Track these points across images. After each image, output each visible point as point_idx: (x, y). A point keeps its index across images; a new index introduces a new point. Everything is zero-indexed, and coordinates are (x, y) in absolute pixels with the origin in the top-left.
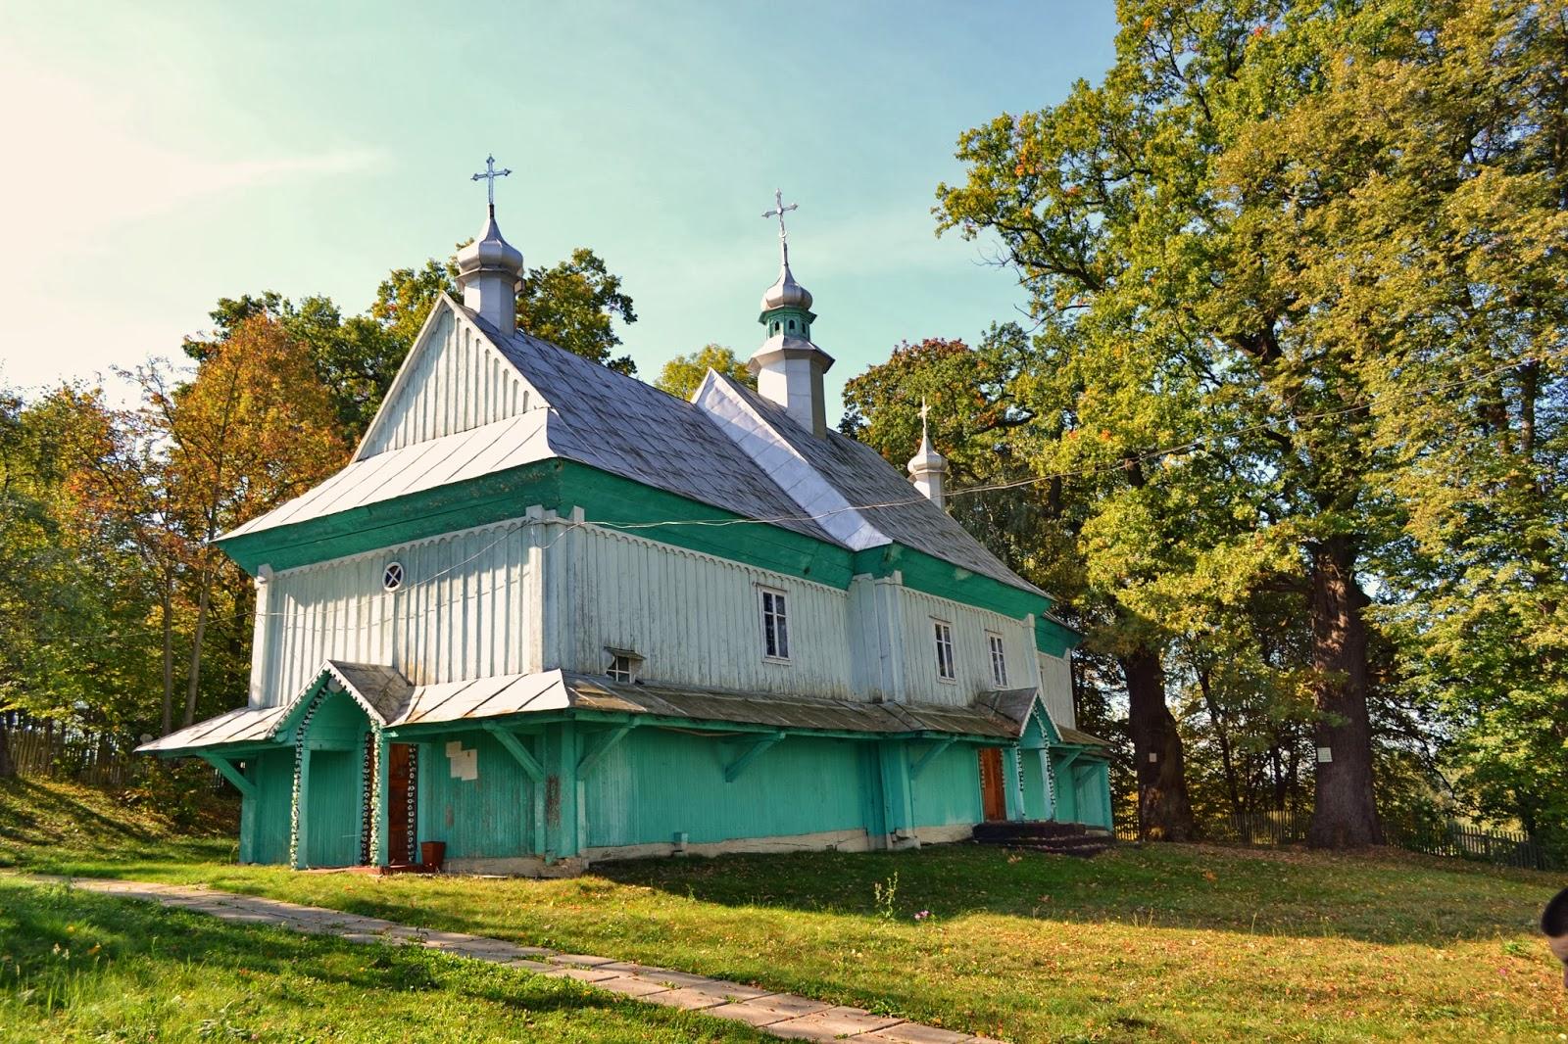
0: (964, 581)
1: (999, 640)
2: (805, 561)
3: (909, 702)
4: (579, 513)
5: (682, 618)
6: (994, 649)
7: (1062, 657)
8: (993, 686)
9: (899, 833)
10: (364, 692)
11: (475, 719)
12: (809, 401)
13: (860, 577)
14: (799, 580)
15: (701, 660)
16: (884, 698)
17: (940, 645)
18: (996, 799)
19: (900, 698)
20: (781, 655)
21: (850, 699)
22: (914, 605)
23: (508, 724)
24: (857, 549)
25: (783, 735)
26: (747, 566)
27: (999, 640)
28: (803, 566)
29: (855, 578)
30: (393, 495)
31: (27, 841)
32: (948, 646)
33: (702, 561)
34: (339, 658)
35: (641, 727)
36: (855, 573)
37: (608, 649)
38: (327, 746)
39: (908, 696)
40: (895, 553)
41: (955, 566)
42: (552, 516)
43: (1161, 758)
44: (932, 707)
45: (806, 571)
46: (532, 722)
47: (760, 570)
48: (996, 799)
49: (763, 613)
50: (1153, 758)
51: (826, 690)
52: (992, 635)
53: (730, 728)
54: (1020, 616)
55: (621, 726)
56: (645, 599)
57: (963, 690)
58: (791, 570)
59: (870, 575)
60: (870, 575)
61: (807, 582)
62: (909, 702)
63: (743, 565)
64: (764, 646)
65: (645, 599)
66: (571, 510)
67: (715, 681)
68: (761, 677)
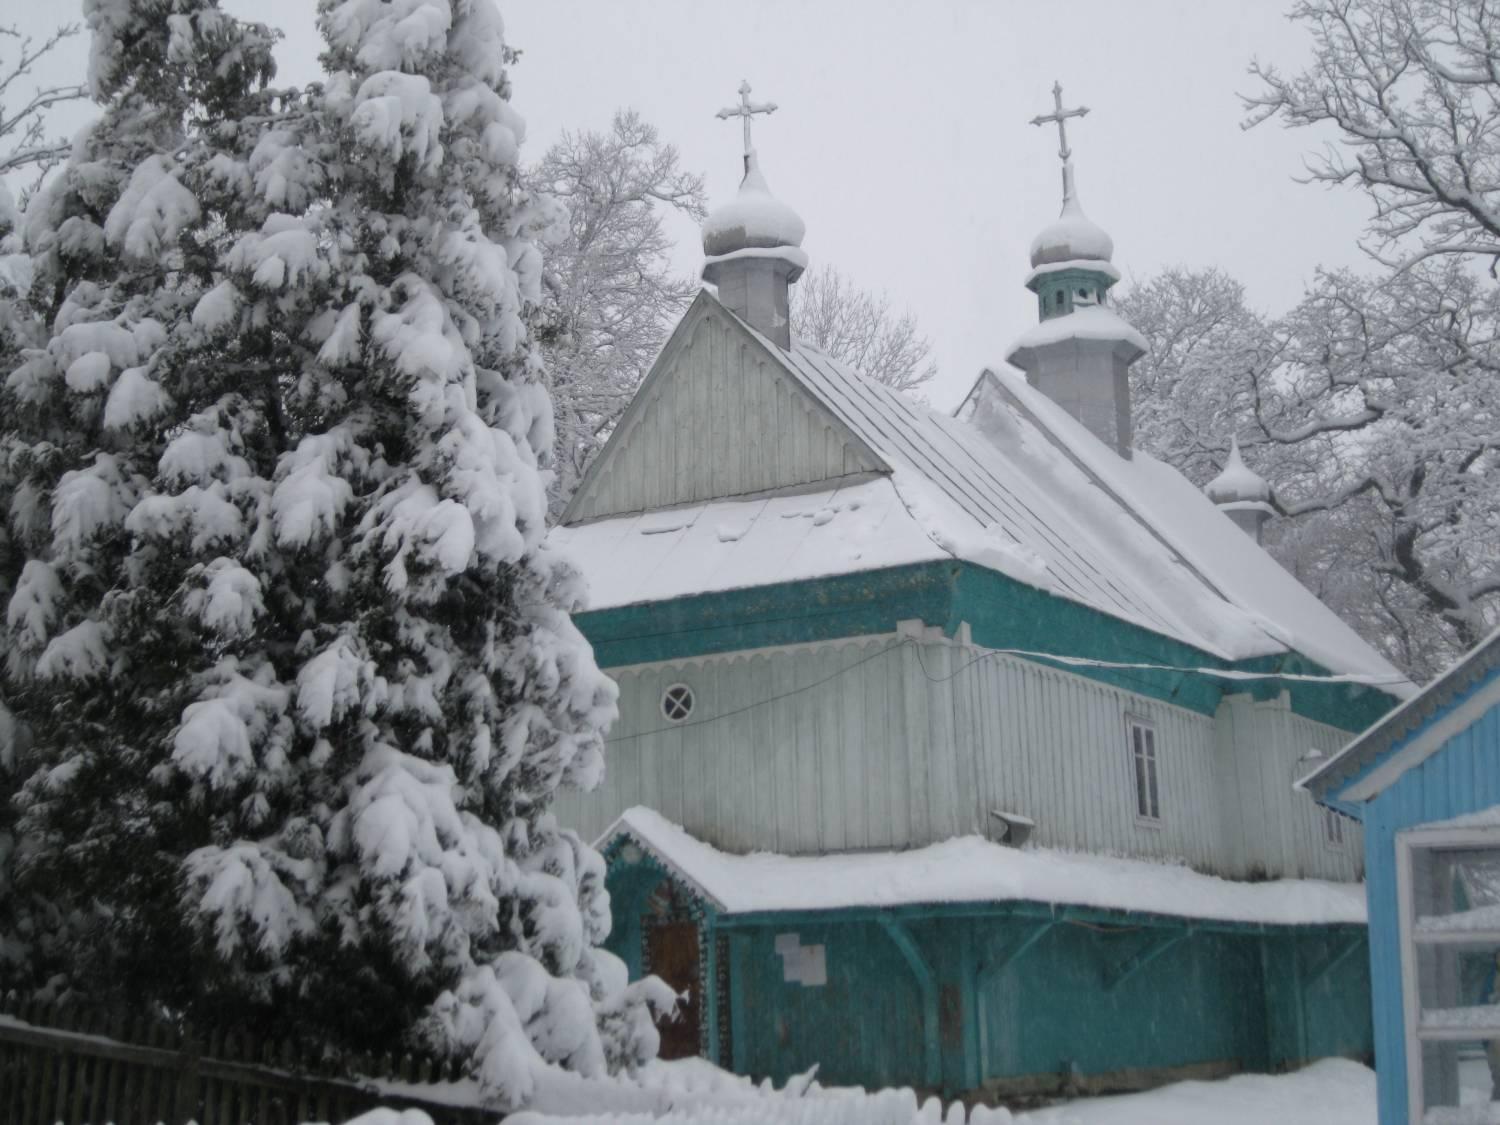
14: (1166, 705)
17: (1139, 762)
29: (1225, 698)
45: (1175, 693)
49: (1133, 756)
61: (1175, 707)
63: (1113, 689)
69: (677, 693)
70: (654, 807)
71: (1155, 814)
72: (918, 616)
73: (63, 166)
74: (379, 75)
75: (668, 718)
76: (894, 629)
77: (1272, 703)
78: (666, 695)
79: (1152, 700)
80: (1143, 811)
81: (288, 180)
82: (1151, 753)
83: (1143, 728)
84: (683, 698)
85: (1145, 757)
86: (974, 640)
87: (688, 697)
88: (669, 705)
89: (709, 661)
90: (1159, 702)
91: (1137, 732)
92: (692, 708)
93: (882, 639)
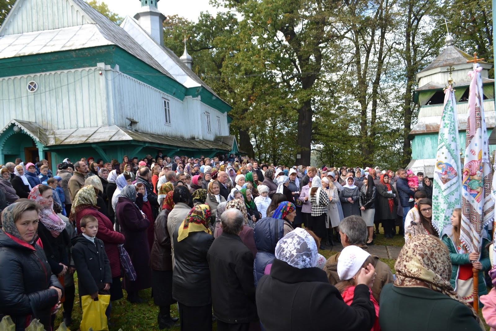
0: (214, 100)
1: (168, 103)
2: (174, 90)
4: (117, 67)
5: (145, 107)
8: (218, 135)
10: (33, 132)
13: (187, 97)
14: (172, 97)
15: (150, 123)
16: (196, 137)
17: (166, 109)
19: (201, 138)
22: (123, 79)
23: (100, 145)
25: (179, 150)
27: (168, 103)
28: (174, 92)
29: (185, 97)
30: (50, 51)
31: (321, 135)
33: (129, 79)
34: (20, 119)
35: (147, 147)
36: (186, 95)
37: (127, 118)
38: (10, 153)
39: (203, 137)
40: (200, 90)
42: (109, 67)
45: (174, 94)
46: (77, 147)
49: (164, 108)
52: (165, 100)
55: (140, 146)
56: (135, 101)
59: (191, 96)
60: (191, 96)
61: (174, 97)
63: (159, 90)
64: (165, 121)
65: (135, 101)
66: (115, 65)
67: (154, 131)
69: (32, 83)
70: (348, 245)
71: (170, 122)
72: (103, 62)
73: (463, 216)
74: (431, 147)
75: (29, 91)
76: (96, 66)
77: (196, 98)
78: (28, 84)
79: (169, 95)
80: (167, 121)
81: (156, 5)
82: (168, 108)
83: (167, 101)
84: (34, 85)
85: (167, 109)
86: (120, 70)
87: (35, 84)
88: (29, 87)
89: (41, 75)
90: (171, 96)
91: (165, 102)
92: (28, 85)
93: (93, 68)
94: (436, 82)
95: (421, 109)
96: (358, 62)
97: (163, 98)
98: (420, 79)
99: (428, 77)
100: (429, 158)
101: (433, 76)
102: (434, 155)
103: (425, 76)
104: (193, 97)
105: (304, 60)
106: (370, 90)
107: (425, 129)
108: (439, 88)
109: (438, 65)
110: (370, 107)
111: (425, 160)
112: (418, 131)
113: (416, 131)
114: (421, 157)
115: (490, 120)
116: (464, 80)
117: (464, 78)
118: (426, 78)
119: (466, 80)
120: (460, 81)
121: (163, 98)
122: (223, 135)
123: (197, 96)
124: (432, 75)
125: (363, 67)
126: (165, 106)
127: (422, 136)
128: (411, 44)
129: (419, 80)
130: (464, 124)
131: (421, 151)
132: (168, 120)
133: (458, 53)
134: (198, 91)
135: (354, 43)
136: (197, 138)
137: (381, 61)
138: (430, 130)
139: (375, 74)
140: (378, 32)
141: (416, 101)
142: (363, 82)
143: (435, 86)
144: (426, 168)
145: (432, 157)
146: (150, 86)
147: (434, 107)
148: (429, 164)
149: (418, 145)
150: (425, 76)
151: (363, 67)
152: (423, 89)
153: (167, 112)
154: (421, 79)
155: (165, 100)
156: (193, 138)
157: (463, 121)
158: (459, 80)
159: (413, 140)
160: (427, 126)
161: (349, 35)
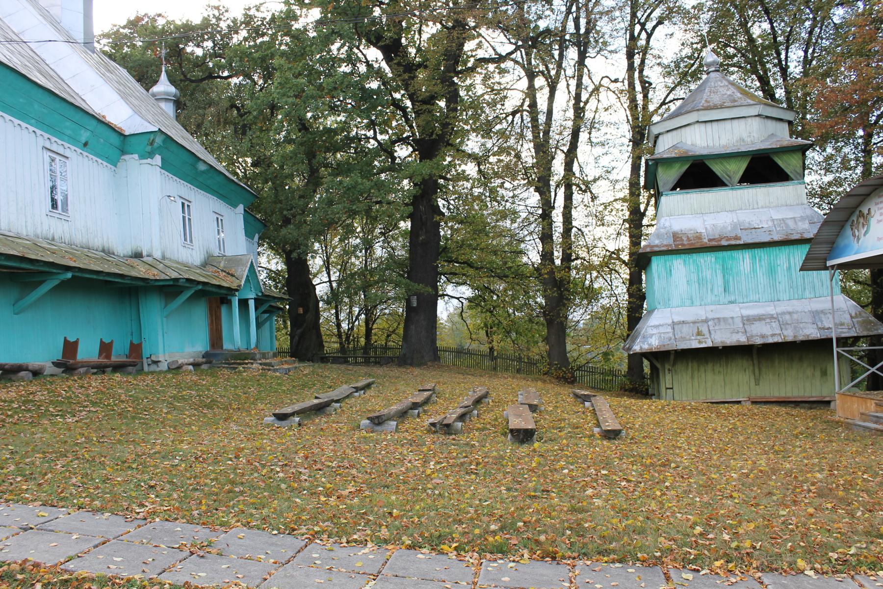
0: (203, 172)
1: (188, 206)
2: (84, 136)
3: (164, 258)
6: (218, 226)
7: (253, 239)
8: (216, 252)
9: (154, 358)
11: (573, 163)
12: (81, 17)
13: (126, 157)
14: (79, 151)
16: (144, 254)
17: (184, 218)
18: (216, 338)
19: (157, 254)
20: (63, 211)
21: (116, 254)
24: (127, 133)
26: (35, 130)
28: (83, 140)
29: (123, 157)
32: (189, 219)
41: (200, 159)
43: (306, 311)
44: (178, 263)
45: (86, 144)
47: (46, 135)
48: (216, 338)
49: (181, 215)
50: (301, 311)
51: (97, 242)
52: (218, 216)
53: (24, 266)
54: (235, 206)
57: (198, 253)
58: (73, 140)
59: (136, 156)
60: (136, 156)
61: (85, 154)
62: (164, 258)
63: (31, 128)
68: (46, 227)
71: (191, 241)
77: (149, 161)
80: (186, 240)
94: (689, 143)
95: (663, 199)
96: (533, 105)
97: (44, 148)
98: (657, 137)
99: (674, 133)
100: (682, 305)
101: (683, 130)
102: (691, 299)
103: (668, 131)
104: (142, 157)
105: (425, 103)
106: (558, 166)
107: (671, 241)
108: (697, 153)
109: (693, 108)
110: (560, 202)
111: (673, 310)
112: (657, 246)
113: (653, 246)
114: (667, 304)
115: (800, 224)
116: (746, 139)
117: (744, 135)
118: (670, 134)
119: (749, 140)
120: (737, 141)
121: (44, 148)
122: (229, 252)
123: (151, 155)
124: (681, 127)
125: (542, 118)
126: (183, 212)
127: (666, 257)
128: (636, 75)
129: (655, 142)
130: (750, 231)
131: (664, 289)
132: (187, 235)
133: (730, 86)
134: (152, 144)
135: (523, 67)
136: (148, 256)
137: (579, 111)
138: (683, 245)
139: (567, 133)
140: (572, 54)
141: (652, 183)
142: (543, 149)
143: (688, 151)
144: (676, 327)
145: (688, 302)
146: (177, 179)
147: (688, 195)
148: (682, 319)
149: (659, 277)
150: (668, 131)
151: (542, 118)
152: (665, 156)
153: (186, 223)
154: (661, 138)
155: (184, 201)
156: (138, 255)
157: (747, 226)
158: (735, 139)
159: (648, 269)
160: (676, 236)
161: (517, 56)
